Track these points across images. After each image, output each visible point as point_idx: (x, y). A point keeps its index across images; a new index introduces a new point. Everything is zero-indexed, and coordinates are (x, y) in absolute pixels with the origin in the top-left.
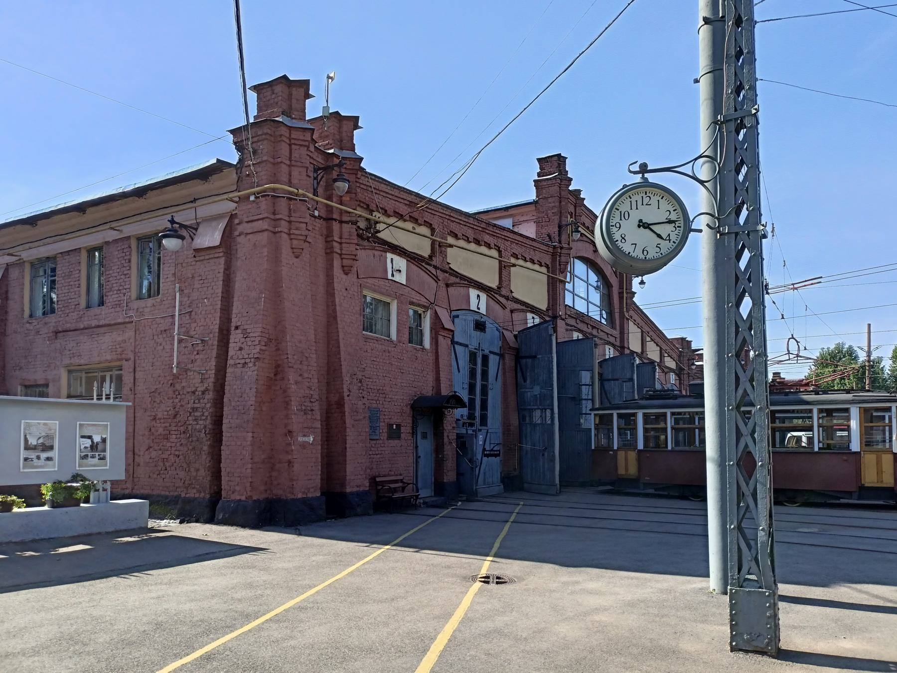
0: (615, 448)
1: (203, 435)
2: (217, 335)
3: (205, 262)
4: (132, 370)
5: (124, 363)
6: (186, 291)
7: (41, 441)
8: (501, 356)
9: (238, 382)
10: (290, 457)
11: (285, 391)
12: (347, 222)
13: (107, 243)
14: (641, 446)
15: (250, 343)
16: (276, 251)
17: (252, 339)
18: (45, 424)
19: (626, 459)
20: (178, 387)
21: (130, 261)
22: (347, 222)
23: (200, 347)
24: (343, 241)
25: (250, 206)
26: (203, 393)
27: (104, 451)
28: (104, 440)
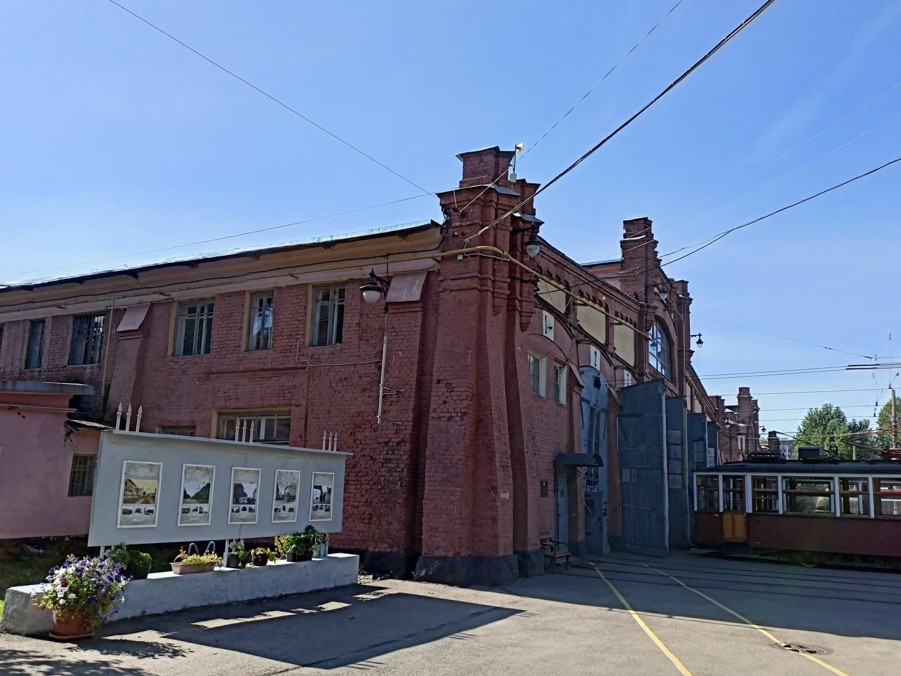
0: (721, 510)
1: (398, 487)
2: (414, 387)
3: (399, 315)
4: (303, 416)
5: (293, 408)
6: (372, 342)
7: (287, 491)
8: (607, 412)
9: (443, 435)
10: (494, 513)
11: (488, 447)
12: (526, 282)
13: (279, 288)
14: (749, 510)
15: (455, 398)
16: (482, 306)
17: (458, 394)
18: (291, 473)
19: (733, 523)
20: (359, 436)
21: (306, 308)
22: (526, 282)
23: (394, 398)
24: (524, 299)
25: (456, 265)
26: (398, 444)
27: (329, 502)
28: (329, 490)
